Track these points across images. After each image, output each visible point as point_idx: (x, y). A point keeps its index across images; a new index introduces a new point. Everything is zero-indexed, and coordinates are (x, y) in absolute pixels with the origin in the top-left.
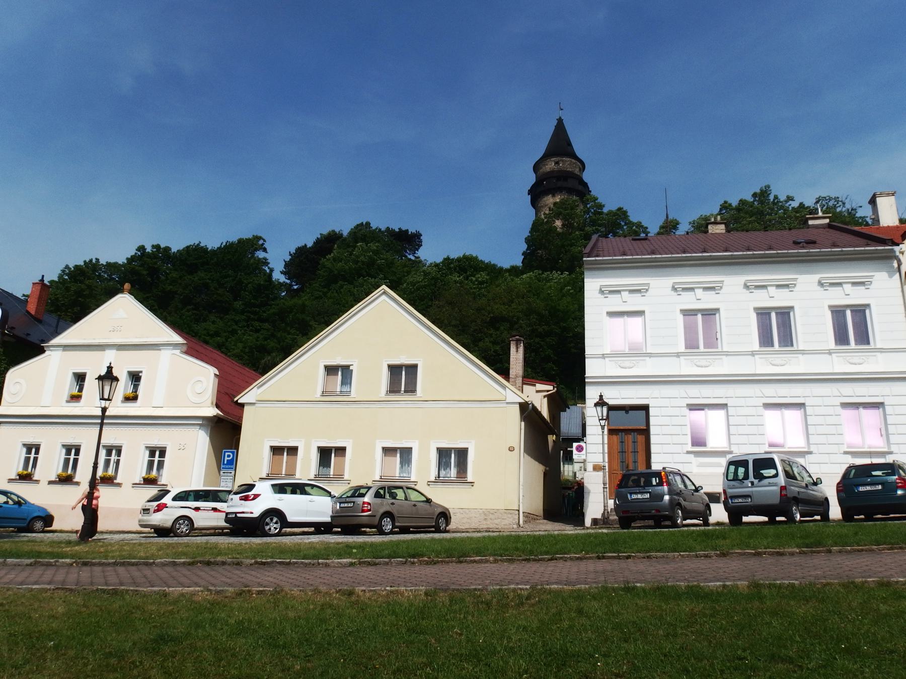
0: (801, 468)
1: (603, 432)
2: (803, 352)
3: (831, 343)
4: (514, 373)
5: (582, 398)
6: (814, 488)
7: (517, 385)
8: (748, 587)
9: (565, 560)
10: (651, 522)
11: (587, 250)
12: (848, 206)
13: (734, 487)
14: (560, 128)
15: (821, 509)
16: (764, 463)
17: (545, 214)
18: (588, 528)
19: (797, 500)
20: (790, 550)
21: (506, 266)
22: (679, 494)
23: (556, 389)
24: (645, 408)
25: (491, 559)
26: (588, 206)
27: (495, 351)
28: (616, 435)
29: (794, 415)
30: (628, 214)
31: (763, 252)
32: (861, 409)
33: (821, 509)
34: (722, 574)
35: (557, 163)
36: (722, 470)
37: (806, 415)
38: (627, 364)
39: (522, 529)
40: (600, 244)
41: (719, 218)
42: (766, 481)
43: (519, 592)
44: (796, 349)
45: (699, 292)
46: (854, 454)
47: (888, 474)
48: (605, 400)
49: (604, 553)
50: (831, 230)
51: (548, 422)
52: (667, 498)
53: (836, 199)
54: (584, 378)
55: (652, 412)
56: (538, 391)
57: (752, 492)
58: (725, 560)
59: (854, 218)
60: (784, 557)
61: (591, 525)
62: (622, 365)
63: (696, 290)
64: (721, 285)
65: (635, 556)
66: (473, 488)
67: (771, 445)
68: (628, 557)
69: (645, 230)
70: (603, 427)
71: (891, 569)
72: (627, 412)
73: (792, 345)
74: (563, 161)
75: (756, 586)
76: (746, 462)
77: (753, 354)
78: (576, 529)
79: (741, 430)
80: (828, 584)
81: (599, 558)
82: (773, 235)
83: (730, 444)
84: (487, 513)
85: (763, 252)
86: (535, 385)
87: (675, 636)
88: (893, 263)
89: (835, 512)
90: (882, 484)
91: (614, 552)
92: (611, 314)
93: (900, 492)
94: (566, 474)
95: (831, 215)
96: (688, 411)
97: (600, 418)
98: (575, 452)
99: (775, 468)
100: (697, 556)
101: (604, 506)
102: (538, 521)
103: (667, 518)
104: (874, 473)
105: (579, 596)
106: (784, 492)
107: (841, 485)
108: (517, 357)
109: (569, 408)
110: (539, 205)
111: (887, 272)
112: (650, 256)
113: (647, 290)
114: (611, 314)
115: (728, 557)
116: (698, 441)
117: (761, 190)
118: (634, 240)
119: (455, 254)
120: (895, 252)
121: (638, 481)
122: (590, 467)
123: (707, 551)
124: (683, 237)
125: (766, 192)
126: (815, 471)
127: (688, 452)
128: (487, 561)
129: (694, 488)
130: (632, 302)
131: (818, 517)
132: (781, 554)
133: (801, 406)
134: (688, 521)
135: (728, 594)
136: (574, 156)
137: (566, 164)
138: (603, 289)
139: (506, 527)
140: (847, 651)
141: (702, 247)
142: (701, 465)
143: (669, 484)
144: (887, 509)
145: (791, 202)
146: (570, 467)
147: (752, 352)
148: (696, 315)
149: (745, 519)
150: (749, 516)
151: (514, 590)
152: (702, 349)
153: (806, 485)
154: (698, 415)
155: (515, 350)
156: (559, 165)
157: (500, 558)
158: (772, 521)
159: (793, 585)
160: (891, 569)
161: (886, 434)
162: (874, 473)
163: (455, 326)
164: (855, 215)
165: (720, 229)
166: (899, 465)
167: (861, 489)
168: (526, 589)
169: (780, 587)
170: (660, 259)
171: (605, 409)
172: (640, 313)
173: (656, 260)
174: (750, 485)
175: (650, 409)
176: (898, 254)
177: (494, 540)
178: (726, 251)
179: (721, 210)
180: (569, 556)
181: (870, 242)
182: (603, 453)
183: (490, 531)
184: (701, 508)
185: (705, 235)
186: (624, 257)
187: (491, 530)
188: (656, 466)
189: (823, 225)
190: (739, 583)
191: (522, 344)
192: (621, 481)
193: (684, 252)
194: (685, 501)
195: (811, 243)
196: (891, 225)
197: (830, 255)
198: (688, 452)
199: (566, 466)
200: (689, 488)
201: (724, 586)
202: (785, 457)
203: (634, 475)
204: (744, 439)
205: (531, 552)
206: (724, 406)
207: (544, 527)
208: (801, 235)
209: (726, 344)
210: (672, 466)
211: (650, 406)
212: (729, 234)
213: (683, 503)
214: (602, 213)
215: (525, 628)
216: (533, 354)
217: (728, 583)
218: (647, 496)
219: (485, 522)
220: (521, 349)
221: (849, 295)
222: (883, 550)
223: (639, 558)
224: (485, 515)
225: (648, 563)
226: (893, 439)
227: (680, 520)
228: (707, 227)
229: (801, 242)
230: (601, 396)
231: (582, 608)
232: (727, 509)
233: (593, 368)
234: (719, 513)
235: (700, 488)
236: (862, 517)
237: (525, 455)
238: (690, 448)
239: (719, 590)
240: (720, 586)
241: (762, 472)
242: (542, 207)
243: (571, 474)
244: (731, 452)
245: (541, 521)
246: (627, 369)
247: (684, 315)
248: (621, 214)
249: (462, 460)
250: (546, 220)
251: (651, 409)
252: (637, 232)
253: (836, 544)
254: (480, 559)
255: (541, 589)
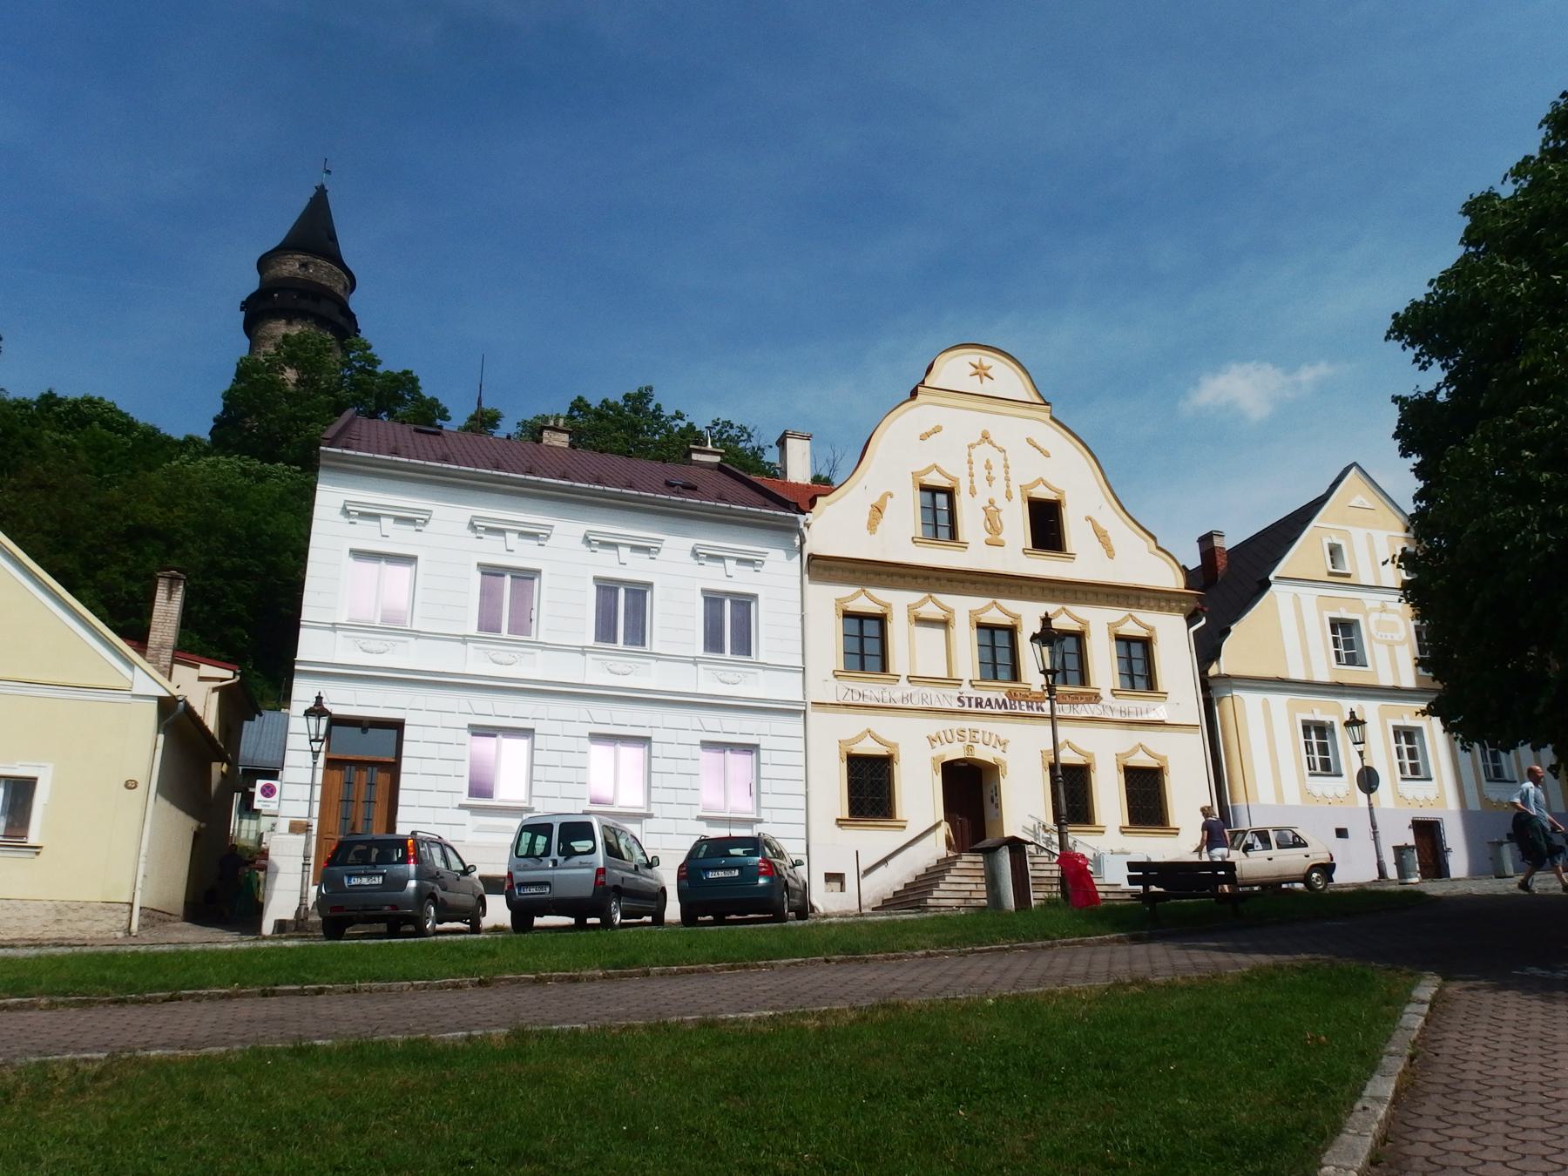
0: (631, 840)
1: (315, 763)
2: (657, 657)
3: (699, 649)
4: (158, 640)
5: (283, 697)
6: (648, 871)
7: (162, 664)
8: (507, 1037)
9: (197, 999)
10: (382, 927)
11: (330, 432)
12: (754, 443)
13: (525, 869)
14: (319, 203)
15: (654, 906)
16: (577, 830)
17: (266, 354)
18: (265, 938)
19: (619, 892)
20: (589, 973)
21: (178, 435)
22: (436, 877)
23: (238, 678)
24: (398, 726)
25: (44, 1001)
26: (351, 356)
27: (129, 593)
28: (340, 770)
29: (632, 756)
30: (420, 384)
31: (619, 490)
32: (728, 753)
33: (654, 906)
34: (473, 1016)
35: (304, 265)
36: (510, 839)
37: (650, 757)
38: (373, 646)
39: (134, 941)
40: (355, 427)
41: (561, 422)
42: (576, 860)
43: (81, 1066)
44: (534, 640)
45: (512, 538)
46: (712, 821)
47: (749, 854)
48: (326, 706)
49: (276, 985)
50: (721, 474)
51: (213, 737)
52: (412, 884)
53: (743, 429)
54: (293, 663)
55: (408, 733)
56: (201, 679)
57: (553, 876)
58: (485, 991)
59: (759, 462)
60: (580, 985)
61: (273, 933)
62: (364, 646)
63: (382, 519)
64: (548, 532)
65: (333, 990)
66: (36, 857)
67: (593, 802)
68: (320, 992)
69: (444, 414)
70: (315, 754)
71: (723, 1000)
72: (364, 730)
73: (643, 644)
74: (316, 264)
75: (519, 1035)
76: (551, 826)
77: (583, 651)
78: (242, 941)
79: (553, 774)
80: (629, 1027)
81: (264, 994)
82: (642, 466)
83: (649, 801)
84: (61, 910)
85: (619, 490)
86: (197, 667)
87: (362, 1131)
88: (795, 539)
89: (673, 911)
90: (740, 868)
91: (295, 983)
92: (358, 554)
93: (762, 881)
94: (243, 835)
95: (723, 451)
96: (469, 735)
97: (313, 737)
98: (258, 796)
99: (593, 838)
100: (440, 987)
101: (301, 898)
102: (170, 925)
103: (409, 919)
104: (732, 851)
105: (204, 1068)
106: (601, 879)
107: (684, 869)
108: (167, 610)
109: (261, 715)
110: (259, 334)
111: (785, 550)
112: (439, 465)
113: (426, 522)
114: (358, 554)
115: (491, 988)
116: (480, 789)
117: (640, 391)
118: (417, 431)
119: (70, 390)
120: (798, 523)
121: (368, 853)
122: (283, 825)
123: (460, 977)
124: (501, 443)
125: (645, 395)
126: (652, 846)
127: (462, 807)
128: (33, 1006)
129: (462, 868)
130: (399, 539)
131: (648, 919)
132: (574, 980)
133: (645, 741)
134: (447, 925)
135: (475, 1050)
136: (337, 260)
137: (320, 271)
138: (349, 508)
139: (100, 936)
140: (630, 1135)
141: (528, 464)
142: (479, 830)
143: (418, 861)
144: (744, 906)
145: (678, 421)
146: (254, 823)
147: (583, 647)
148: (503, 576)
149: (538, 921)
150: (546, 917)
151: (73, 1063)
152: (505, 633)
153: (636, 867)
154: (486, 745)
155: (165, 596)
156: (307, 269)
157: (61, 999)
158: (581, 925)
159: (576, 1032)
160: (723, 1000)
161: (756, 792)
162: (732, 851)
163: (49, 533)
164: (761, 457)
165: (561, 440)
166: (765, 840)
167: (712, 875)
168: (100, 1060)
169: (557, 1034)
170: (453, 473)
171: (324, 722)
172: (410, 560)
173: (446, 473)
174: (550, 866)
175: (406, 728)
176: (802, 526)
177: (59, 962)
178: (564, 478)
179: (571, 410)
180: (206, 992)
181: (768, 502)
182: (311, 802)
183: (62, 945)
184: (470, 901)
185: (536, 445)
186: (394, 458)
187: (66, 942)
188: (402, 830)
189: (710, 463)
190: (494, 1032)
191: (181, 587)
192: (335, 853)
193: (497, 468)
194: (444, 889)
195: (690, 488)
196: (801, 482)
197: (697, 510)
198: (462, 807)
199: (245, 822)
200: (454, 868)
201: (469, 1038)
202: (610, 822)
203: (360, 842)
204: (552, 789)
205: (130, 987)
206: (528, 733)
207: (181, 936)
208: (677, 473)
209: (544, 629)
210: (428, 829)
211: (406, 723)
212: (573, 451)
213: (440, 894)
214: (372, 374)
215: (75, 1139)
216: (206, 608)
217: (474, 1033)
218: (379, 880)
219: (56, 927)
220: (178, 596)
221: (731, 577)
222: (722, 970)
223: (338, 993)
224: (58, 911)
225: (352, 1002)
226: (765, 800)
227: (430, 922)
228: (541, 434)
229: (676, 484)
230: (319, 698)
231: (202, 1093)
232: (510, 904)
233: (311, 646)
234: (497, 912)
235: (472, 869)
236: (709, 917)
237: (159, 797)
238: (464, 799)
239: (460, 1044)
240: (462, 1037)
241: (572, 844)
242: (264, 338)
243: (252, 836)
244: (530, 810)
245: (178, 925)
246: (730, 686)
247: (483, 573)
248: (407, 381)
249: (20, 801)
250: (267, 364)
251: (407, 728)
252: (427, 416)
253: (657, 962)
254: (18, 1002)
255: (128, 1059)
